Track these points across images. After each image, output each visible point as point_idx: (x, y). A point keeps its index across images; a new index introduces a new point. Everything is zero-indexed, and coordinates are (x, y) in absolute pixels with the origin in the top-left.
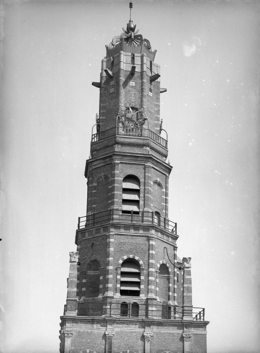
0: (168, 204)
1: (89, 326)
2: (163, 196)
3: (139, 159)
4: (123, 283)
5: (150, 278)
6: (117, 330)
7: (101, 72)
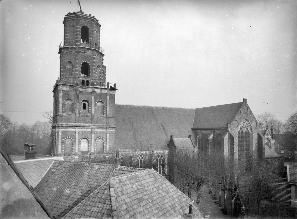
5: (94, 71)
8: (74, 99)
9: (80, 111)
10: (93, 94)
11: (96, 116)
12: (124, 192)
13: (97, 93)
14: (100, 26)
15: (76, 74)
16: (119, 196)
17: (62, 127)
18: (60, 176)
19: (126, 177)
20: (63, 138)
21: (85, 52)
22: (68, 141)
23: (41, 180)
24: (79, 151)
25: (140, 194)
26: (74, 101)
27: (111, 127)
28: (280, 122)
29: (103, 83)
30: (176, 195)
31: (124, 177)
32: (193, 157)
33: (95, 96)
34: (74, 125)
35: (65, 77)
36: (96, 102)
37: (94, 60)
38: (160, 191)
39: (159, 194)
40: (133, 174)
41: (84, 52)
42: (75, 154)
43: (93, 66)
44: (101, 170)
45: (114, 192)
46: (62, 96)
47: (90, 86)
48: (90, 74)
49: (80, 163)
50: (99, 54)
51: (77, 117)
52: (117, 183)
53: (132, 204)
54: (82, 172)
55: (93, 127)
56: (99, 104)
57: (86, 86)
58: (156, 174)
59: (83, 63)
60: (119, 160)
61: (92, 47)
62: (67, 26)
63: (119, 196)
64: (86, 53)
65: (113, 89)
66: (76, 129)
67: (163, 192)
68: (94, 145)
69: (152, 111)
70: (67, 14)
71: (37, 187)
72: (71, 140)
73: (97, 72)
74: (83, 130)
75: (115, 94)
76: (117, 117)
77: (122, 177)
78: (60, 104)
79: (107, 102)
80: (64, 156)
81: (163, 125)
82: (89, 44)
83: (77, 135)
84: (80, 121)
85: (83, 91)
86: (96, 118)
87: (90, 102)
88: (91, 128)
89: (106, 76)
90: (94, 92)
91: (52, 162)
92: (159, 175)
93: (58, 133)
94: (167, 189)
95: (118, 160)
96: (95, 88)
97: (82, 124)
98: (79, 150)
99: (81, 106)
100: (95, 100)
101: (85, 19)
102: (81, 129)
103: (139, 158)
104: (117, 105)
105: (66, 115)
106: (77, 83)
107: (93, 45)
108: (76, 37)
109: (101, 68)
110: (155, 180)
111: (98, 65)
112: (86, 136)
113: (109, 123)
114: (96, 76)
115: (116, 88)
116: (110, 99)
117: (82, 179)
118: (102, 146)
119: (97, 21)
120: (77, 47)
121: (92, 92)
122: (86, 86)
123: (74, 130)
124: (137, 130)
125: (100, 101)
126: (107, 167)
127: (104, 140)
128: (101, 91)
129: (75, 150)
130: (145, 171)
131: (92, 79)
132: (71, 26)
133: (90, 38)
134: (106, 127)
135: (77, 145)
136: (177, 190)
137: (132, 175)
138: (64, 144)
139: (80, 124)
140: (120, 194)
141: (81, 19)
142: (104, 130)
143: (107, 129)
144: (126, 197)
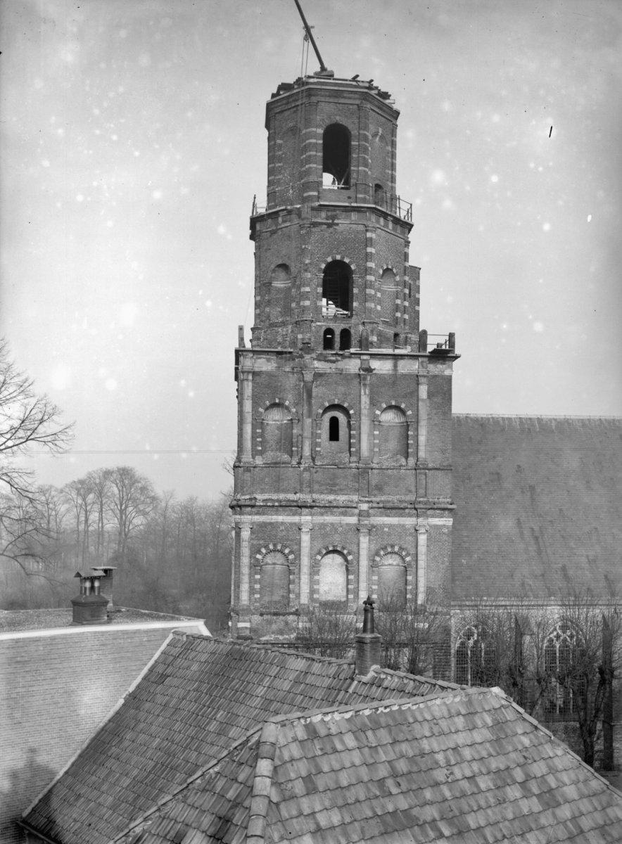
0: (395, 171)
2: (387, 171)
5: (368, 291)
7: (320, 66)
8: (296, 405)
9: (318, 449)
10: (365, 379)
11: (374, 466)
12: (321, 782)
13: (381, 377)
14: (396, 114)
15: (304, 309)
16: (294, 797)
17: (254, 510)
18: (181, 692)
19: (348, 716)
20: (255, 550)
21: (336, 221)
22: (274, 563)
23: (122, 701)
24: (312, 599)
25: (401, 797)
26: (294, 410)
27: (435, 507)
29: (409, 335)
30: (595, 814)
31: (337, 716)
33: (372, 386)
34: (293, 501)
35: (267, 323)
36: (378, 412)
37: (369, 250)
38: (513, 792)
39: (505, 801)
40: (386, 708)
41: (331, 221)
42: (297, 610)
43: (367, 271)
44: (310, 679)
45: (268, 777)
46: (253, 395)
47: (352, 350)
48: (355, 304)
49: (247, 649)
50: (391, 225)
51: (305, 469)
52: (295, 739)
54: (249, 683)
55: (364, 507)
56: (389, 417)
57: (341, 352)
58: (510, 715)
59: (329, 266)
60: (371, 642)
61: (364, 200)
62: (275, 133)
63: (294, 797)
64: (337, 224)
65: (444, 355)
66: (300, 514)
67: (527, 794)
68: (369, 579)
70: (275, 92)
71: (108, 727)
72: (286, 556)
73: (383, 292)
74: (329, 519)
75: (451, 376)
76: (470, 466)
77: (327, 718)
78: (244, 425)
79: (418, 409)
80: (261, 618)
82: (353, 189)
83: (305, 539)
84: (316, 487)
85: (329, 371)
86: (375, 471)
87: (351, 412)
88: (356, 511)
89: (422, 309)
90: (369, 370)
91: (165, 637)
92: (524, 720)
93: (238, 530)
94: (553, 785)
95: (368, 641)
96: (373, 356)
97: (322, 496)
98: (316, 596)
99: (320, 429)
100: (373, 403)
101: (336, 97)
102: (322, 514)
103: (558, 637)
104: (471, 419)
105: (268, 465)
106: (307, 341)
107: (366, 192)
108: (304, 169)
109: (398, 278)
110: (498, 740)
111: (387, 265)
112: (337, 541)
113: (429, 492)
114: (379, 308)
115: (453, 351)
116: (430, 395)
117: (241, 710)
118: (401, 585)
119: (386, 95)
120: (306, 211)
121: (362, 372)
122: (341, 352)
123: (296, 519)
124: (549, 519)
125: (390, 407)
126: (333, 670)
127: (408, 559)
128: (395, 366)
129: (298, 596)
130: (450, 694)
131: (364, 323)
132: (290, 133)
133: (355, 169)
134: (416, 509)
135: (305, 578)
136: (609, 791)
137: (380, 709)
138: (261, 572)
139: (315, 496)
140: (299, 787)
141: (323, 99)
142: (409, 521)
143: (418, 516)
144: (327, 803)
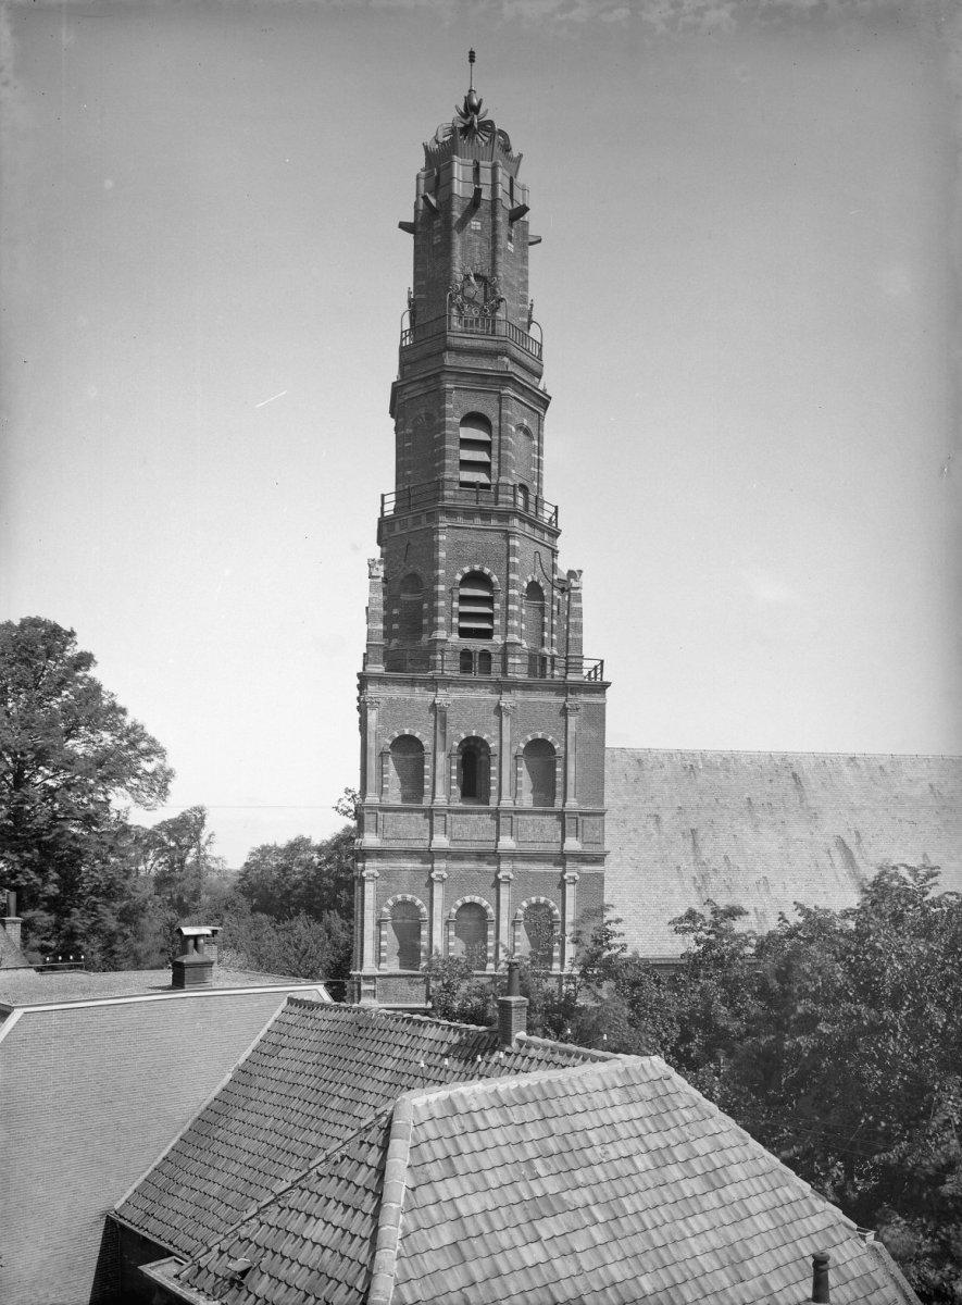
1: (407, 689)
3: (489, 381)
4: (463, 616)
6: (455, 696)
28: (93, 672)
32: (223, 874)
53: (489, 1222)
69: (795, 776)
81: (850, 841)
